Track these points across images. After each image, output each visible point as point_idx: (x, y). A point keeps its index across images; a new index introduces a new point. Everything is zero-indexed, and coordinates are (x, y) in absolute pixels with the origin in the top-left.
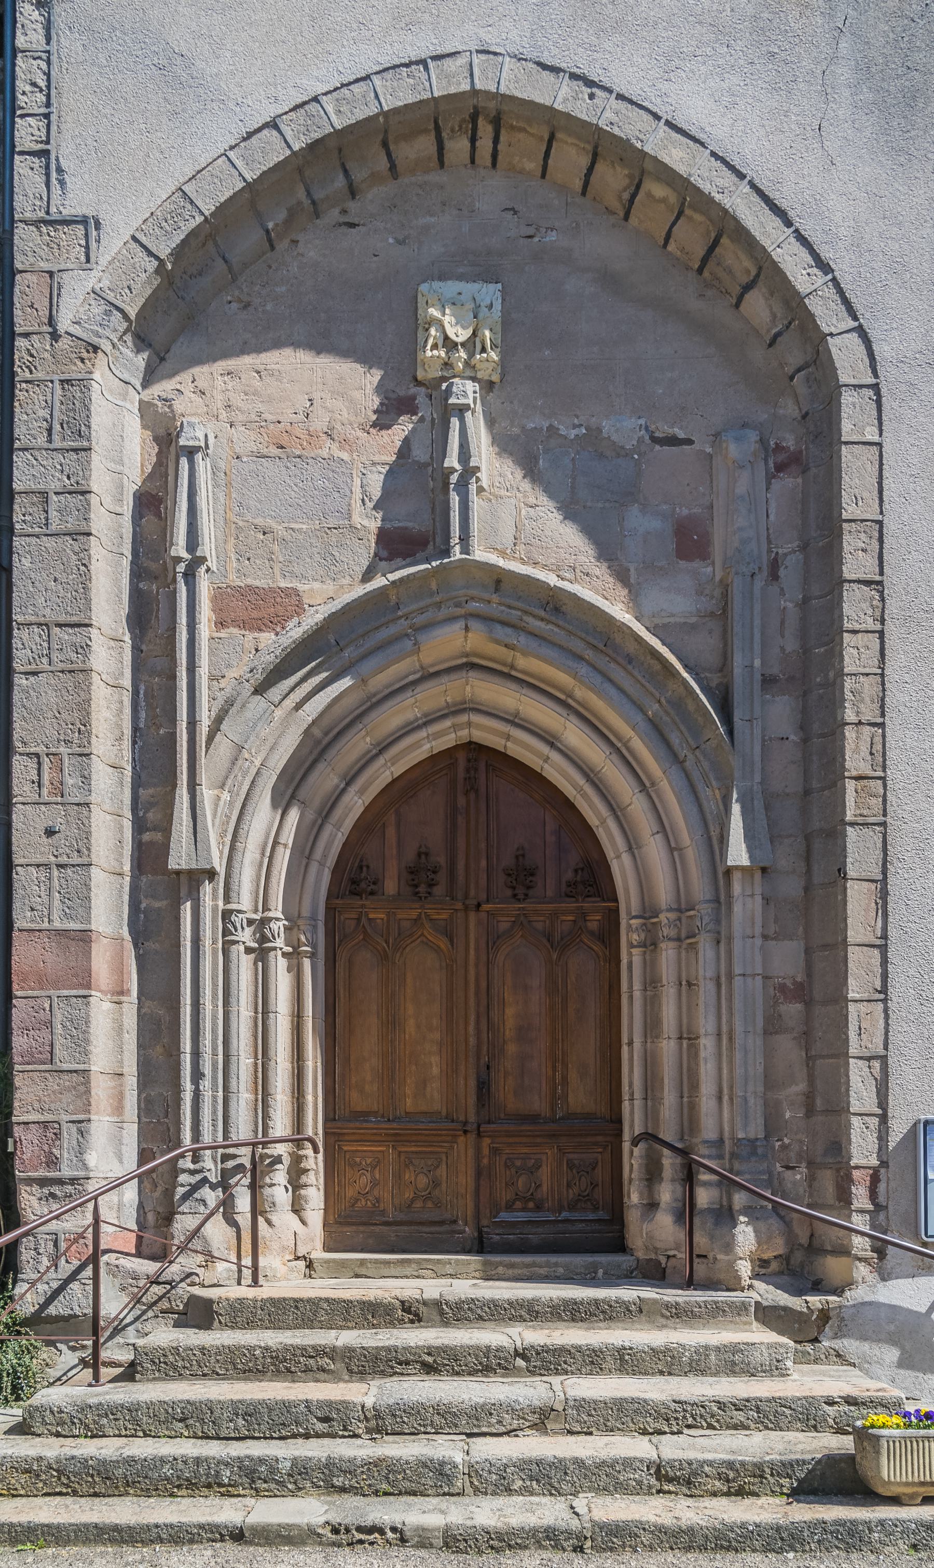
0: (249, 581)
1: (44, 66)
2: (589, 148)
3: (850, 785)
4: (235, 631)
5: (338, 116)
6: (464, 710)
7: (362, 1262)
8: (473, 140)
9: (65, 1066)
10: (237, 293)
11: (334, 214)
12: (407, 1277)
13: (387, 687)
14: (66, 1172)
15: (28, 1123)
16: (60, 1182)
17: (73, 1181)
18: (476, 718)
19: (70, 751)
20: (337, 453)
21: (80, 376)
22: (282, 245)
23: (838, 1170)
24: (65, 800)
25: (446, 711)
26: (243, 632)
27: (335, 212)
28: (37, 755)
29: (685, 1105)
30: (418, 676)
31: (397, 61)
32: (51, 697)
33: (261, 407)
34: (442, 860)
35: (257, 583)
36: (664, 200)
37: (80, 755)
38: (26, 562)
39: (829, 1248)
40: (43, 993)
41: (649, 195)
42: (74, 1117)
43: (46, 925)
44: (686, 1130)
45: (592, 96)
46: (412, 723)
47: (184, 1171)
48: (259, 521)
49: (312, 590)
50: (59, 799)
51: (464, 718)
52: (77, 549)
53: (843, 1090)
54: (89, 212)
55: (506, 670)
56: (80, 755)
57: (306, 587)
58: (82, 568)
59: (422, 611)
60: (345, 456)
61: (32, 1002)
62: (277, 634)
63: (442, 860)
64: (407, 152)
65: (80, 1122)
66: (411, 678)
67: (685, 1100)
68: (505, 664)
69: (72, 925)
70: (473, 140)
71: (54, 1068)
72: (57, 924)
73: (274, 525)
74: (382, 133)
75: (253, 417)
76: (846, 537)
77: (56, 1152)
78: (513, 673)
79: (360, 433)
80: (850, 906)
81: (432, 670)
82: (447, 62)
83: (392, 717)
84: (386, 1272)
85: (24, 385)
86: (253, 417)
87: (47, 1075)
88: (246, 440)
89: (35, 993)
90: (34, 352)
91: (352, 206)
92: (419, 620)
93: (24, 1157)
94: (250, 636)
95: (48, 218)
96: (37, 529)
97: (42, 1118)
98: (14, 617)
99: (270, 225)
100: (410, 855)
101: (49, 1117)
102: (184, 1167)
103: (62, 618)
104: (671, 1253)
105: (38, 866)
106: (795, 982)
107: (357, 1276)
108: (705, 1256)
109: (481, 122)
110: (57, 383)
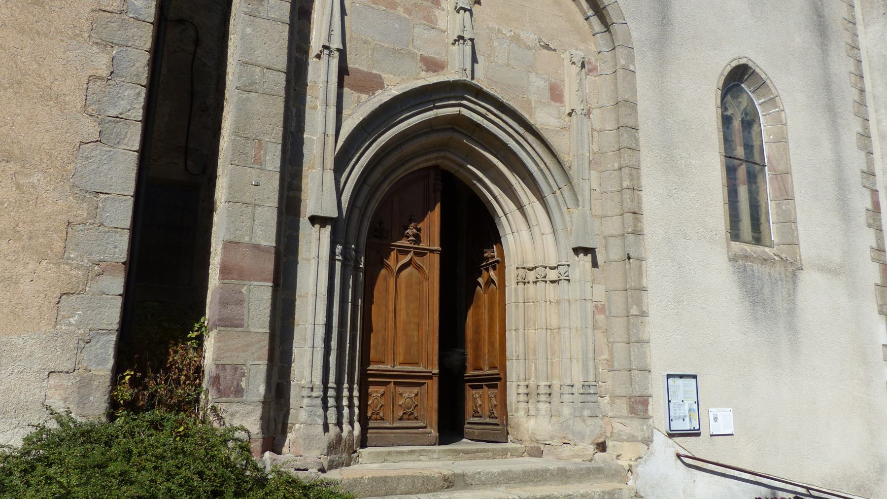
35: (361, 68)
39: (625, 438)
51: (442, 154)
60: (407, 16)
77: (243, 384)
84: (405, 458)
94: (356, 95)
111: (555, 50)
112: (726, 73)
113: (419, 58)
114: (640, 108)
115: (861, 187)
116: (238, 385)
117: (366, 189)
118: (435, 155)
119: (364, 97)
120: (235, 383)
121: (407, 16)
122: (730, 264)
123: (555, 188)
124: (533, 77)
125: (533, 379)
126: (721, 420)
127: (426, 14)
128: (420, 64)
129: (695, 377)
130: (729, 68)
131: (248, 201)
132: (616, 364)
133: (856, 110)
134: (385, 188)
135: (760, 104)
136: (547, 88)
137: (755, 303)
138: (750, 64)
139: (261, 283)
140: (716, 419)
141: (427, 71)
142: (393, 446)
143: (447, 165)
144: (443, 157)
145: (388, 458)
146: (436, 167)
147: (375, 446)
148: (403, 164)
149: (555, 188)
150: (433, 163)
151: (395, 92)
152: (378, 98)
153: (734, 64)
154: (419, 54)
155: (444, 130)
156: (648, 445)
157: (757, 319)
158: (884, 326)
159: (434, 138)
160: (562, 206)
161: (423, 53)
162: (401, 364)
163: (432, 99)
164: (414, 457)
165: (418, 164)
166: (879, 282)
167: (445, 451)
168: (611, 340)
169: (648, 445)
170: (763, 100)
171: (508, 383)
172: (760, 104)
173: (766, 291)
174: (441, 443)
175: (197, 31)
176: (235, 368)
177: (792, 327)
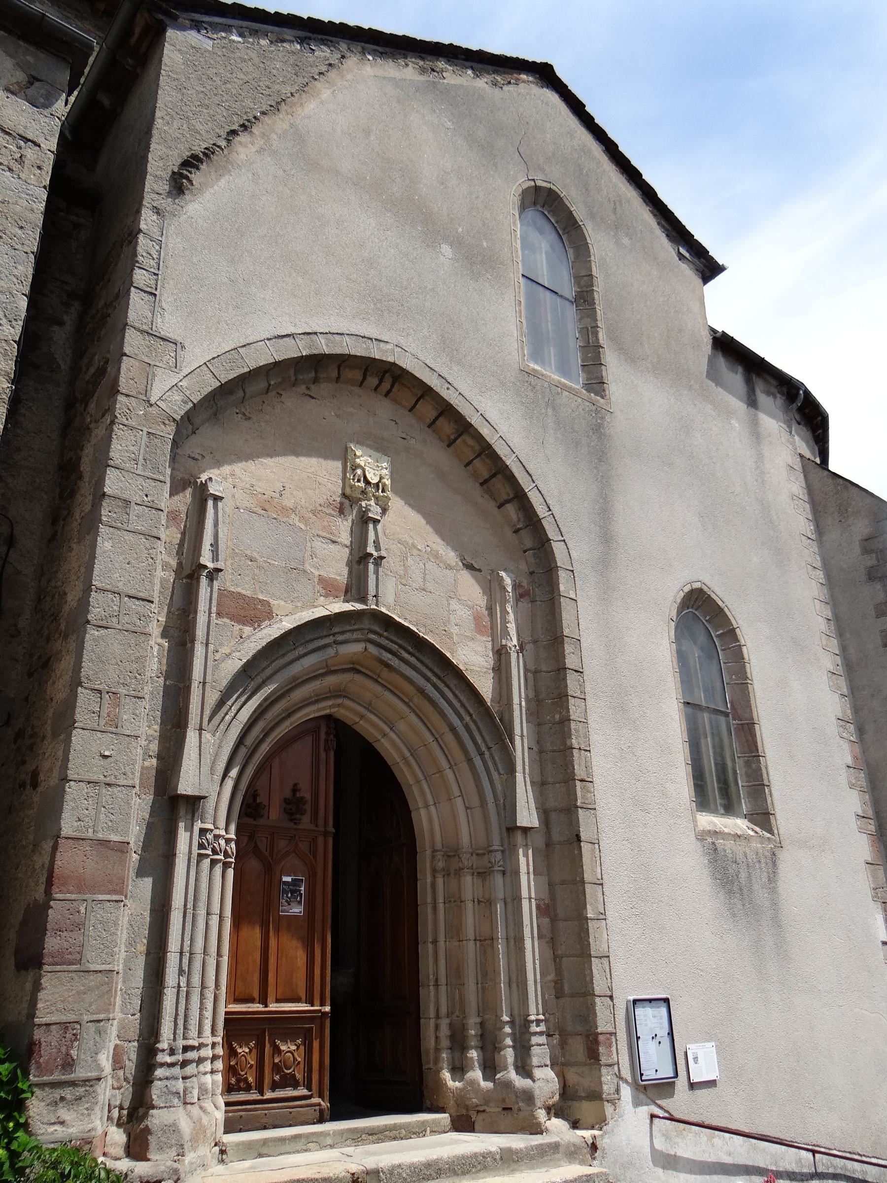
0: (239, 590)
1: (158, 247)
2: (440, 409)
3: (578, 783)
4: (228, 621)
5: (324, 347)
6: (339, 696)
7: (265, 1142)
8: (381, 381)
9: (93, 967)
10: (243, 410)
11: (303, 388)
12: (298, 1152)
13: (306, 674)
14: (80, 1073)
15: (49, 1025)
16: (73, 1084)
17: (86, 1081)
18: (347, 702)
19: (127, 693)
20: (298, 524)
21: (161, 434)
22: (272, 394)
23: (587, 1036)
24: (119, 730)
25: (328, 695)
26: (233, 623)
27: (303, 387)
28: (100, 692)
29: (480, 989)
30: (324, 671)
31: (357, 333)
32: (116, 648)
33: (254, 482)
34: (308, 796)
35: (244, 592)
36: (472, 447)
37: (135, 697)
38: (108, 545)
39: (583, 1094)
40: (80, 897)
41: (464, 441)
42: (95, 1017)
43: (90, 834)
44: (481, 1010)
45: (448, 389)
46: (308, 699)
47: (162, 1065)
48: (248, 552)
49: (279, 605)
50: (114, 730)
51: (340, 701)
52: (148, 546)
53: (588, 979)
54: (179, 339)
55: (375, 677)
56: (135, 697)
57: (276, 602)
58: (150, 560)
59: (343, 633)
60: (303, 526)
61: (67, 905)
62: (255, 629)
63: (308, 796)
64: (348, 374)
65: (99, 1021)
66: (321, 671)
67: (479, 985)
68: (375, 674)
69: (114, 838)
70: (381, 381)
71: (83, 968)
72: (100, 836)
73: (258, 557)
74: (343, 361)
75: (248, 486)
76: (566, 646)
77: (74, 1053)
78: (379, 680)
79: (311, 515)
80: (584, 859)
81: (332, 669)
82: (382, 344)
83: (299, 694)
84: (288, 1147)
85: (121, 426)
86: (248, 486)
87: (73, 975)
88: (245, 501)
89: (73, 896)
90: (131, 408)
91: (312, 387)
92: (340, 638)
93: (41, 1060)
94: (238, 627)
95: (150, 331)
96: (120, 525)
97: (63, 1018)
98: (94, 583)
99: (272, 383)
100: (288, 793)
101: (72, 1017)
102: (163, 1061)
103: (132, 592)
104: (481, 1109)
105: (89, 783)
106: (545, 904)
107: (261, 1155)
108: (511, 1109)
109: (387, 375)
110: (145, 433)
111: (480, 570)
112: (679, 601)
113: (316, 580)
114: (584, 645)
115: (838, 737)
116: (68, 1054)
117: (243, 752)
118: (330, 703)
119: (247, 630)
120: (64, 1049)
121: (303, 526)
122: (699, 843)
123: (484, 748)
124: (454, 605)
125: (457, 1013)
126: (704, 1063)
127: (326, 523)
128: (318, 587)
129: (666, 1001)
130: (682, 594)
131: (94, 778)
132: (566, 987)
133: (824, 643)
134: (265, 748)
135: (718, 636)
136: (471, 618)
137: (730, 892)
138: (705, 589)
139: (108, 897)
140: (696, 1059)
141: (326, 596)
142: (265, 1128)
143: (347, 712)
144: (339, 705)
145: (264, 1150)
146: (328, 717)
147: (240, 1131)
148: (289, 716)
149: (484, 748)
150: (327, 711)
151: (288, 624)
152: (265, 631)
153: (687, 589)
154: (317, 573)
155: (344, 671)
156: (614, 1104)
157: (734, 916)
158: (880, 918)
159: (331, 681)
160: (493, 771)
161: (322, 573)
162: (278, 1001)
163: (332, 632)
164: (299, 1145)
165: (308, 714)
166: (870, 860)
167: (342, 1132)
168: (560, 952)
169: (614, 1104)
170: (721, 631)
171: (422, 1021)
172: (718, 636)
173: (743, 875)
174: (336, 1116)
175: (13, 529)
176: (65, 1026)
177: (777, 923)
